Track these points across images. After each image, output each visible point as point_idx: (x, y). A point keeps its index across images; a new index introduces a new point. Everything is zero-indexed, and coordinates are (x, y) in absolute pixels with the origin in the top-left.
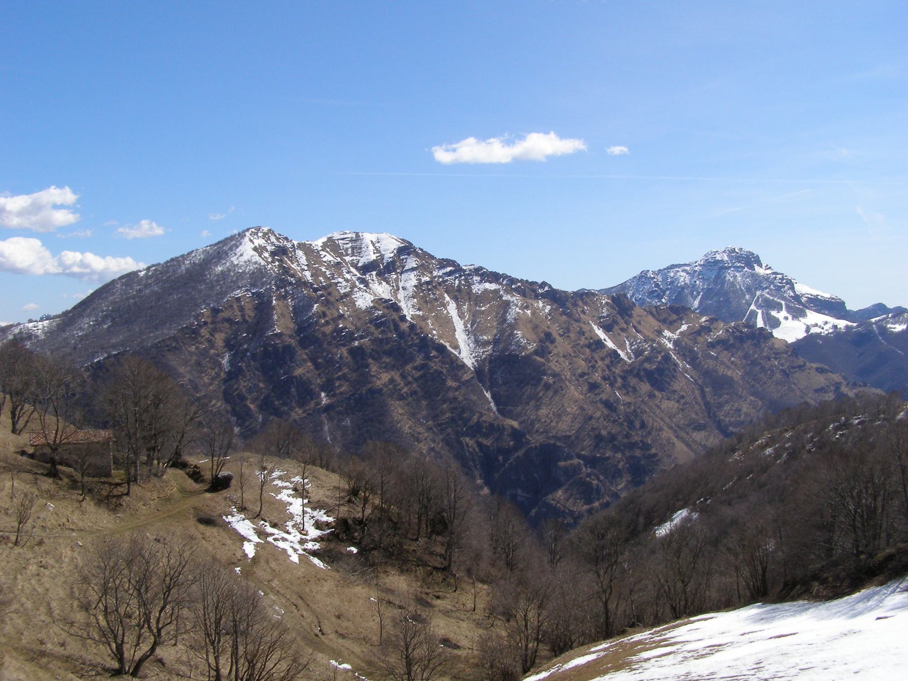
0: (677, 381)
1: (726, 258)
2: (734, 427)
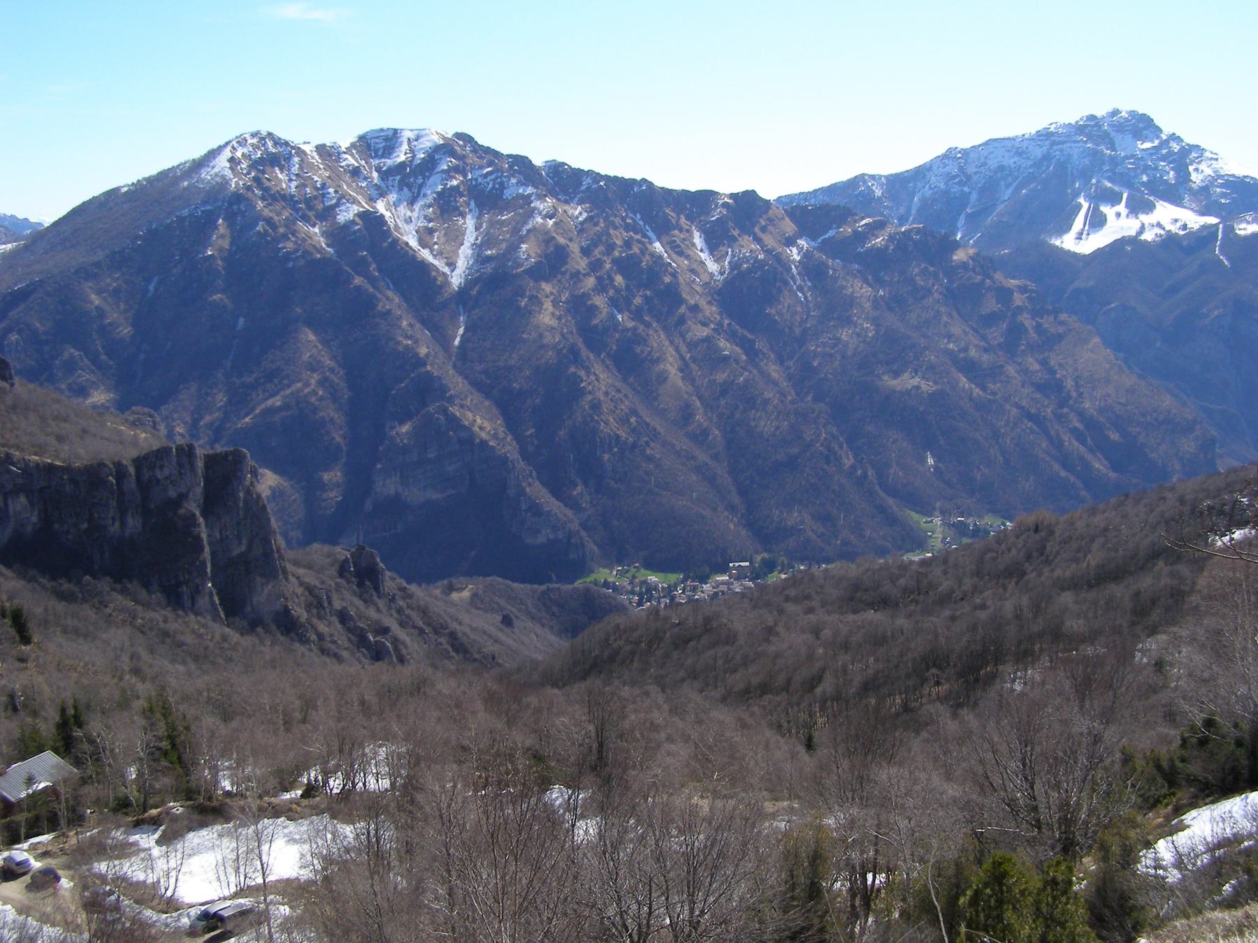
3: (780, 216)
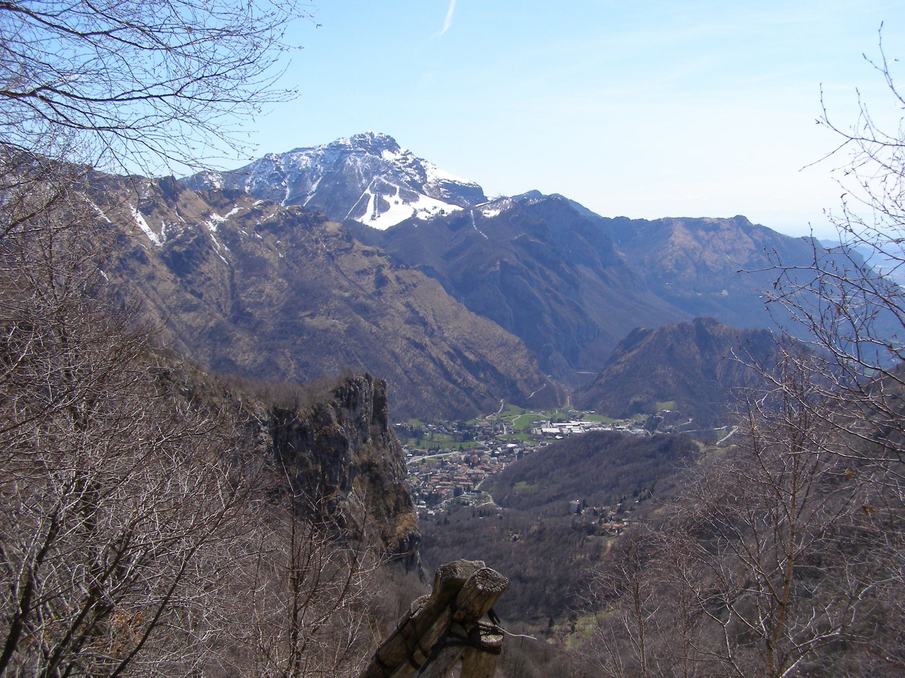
0: (207, 264)
1: (349, 143)
2: (251, 308)
3: (194, 197)
